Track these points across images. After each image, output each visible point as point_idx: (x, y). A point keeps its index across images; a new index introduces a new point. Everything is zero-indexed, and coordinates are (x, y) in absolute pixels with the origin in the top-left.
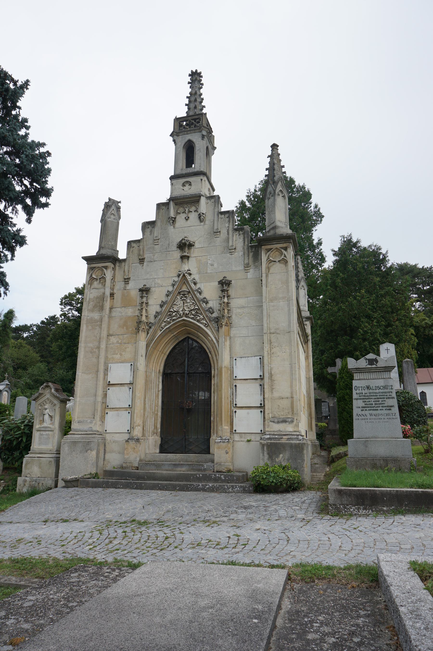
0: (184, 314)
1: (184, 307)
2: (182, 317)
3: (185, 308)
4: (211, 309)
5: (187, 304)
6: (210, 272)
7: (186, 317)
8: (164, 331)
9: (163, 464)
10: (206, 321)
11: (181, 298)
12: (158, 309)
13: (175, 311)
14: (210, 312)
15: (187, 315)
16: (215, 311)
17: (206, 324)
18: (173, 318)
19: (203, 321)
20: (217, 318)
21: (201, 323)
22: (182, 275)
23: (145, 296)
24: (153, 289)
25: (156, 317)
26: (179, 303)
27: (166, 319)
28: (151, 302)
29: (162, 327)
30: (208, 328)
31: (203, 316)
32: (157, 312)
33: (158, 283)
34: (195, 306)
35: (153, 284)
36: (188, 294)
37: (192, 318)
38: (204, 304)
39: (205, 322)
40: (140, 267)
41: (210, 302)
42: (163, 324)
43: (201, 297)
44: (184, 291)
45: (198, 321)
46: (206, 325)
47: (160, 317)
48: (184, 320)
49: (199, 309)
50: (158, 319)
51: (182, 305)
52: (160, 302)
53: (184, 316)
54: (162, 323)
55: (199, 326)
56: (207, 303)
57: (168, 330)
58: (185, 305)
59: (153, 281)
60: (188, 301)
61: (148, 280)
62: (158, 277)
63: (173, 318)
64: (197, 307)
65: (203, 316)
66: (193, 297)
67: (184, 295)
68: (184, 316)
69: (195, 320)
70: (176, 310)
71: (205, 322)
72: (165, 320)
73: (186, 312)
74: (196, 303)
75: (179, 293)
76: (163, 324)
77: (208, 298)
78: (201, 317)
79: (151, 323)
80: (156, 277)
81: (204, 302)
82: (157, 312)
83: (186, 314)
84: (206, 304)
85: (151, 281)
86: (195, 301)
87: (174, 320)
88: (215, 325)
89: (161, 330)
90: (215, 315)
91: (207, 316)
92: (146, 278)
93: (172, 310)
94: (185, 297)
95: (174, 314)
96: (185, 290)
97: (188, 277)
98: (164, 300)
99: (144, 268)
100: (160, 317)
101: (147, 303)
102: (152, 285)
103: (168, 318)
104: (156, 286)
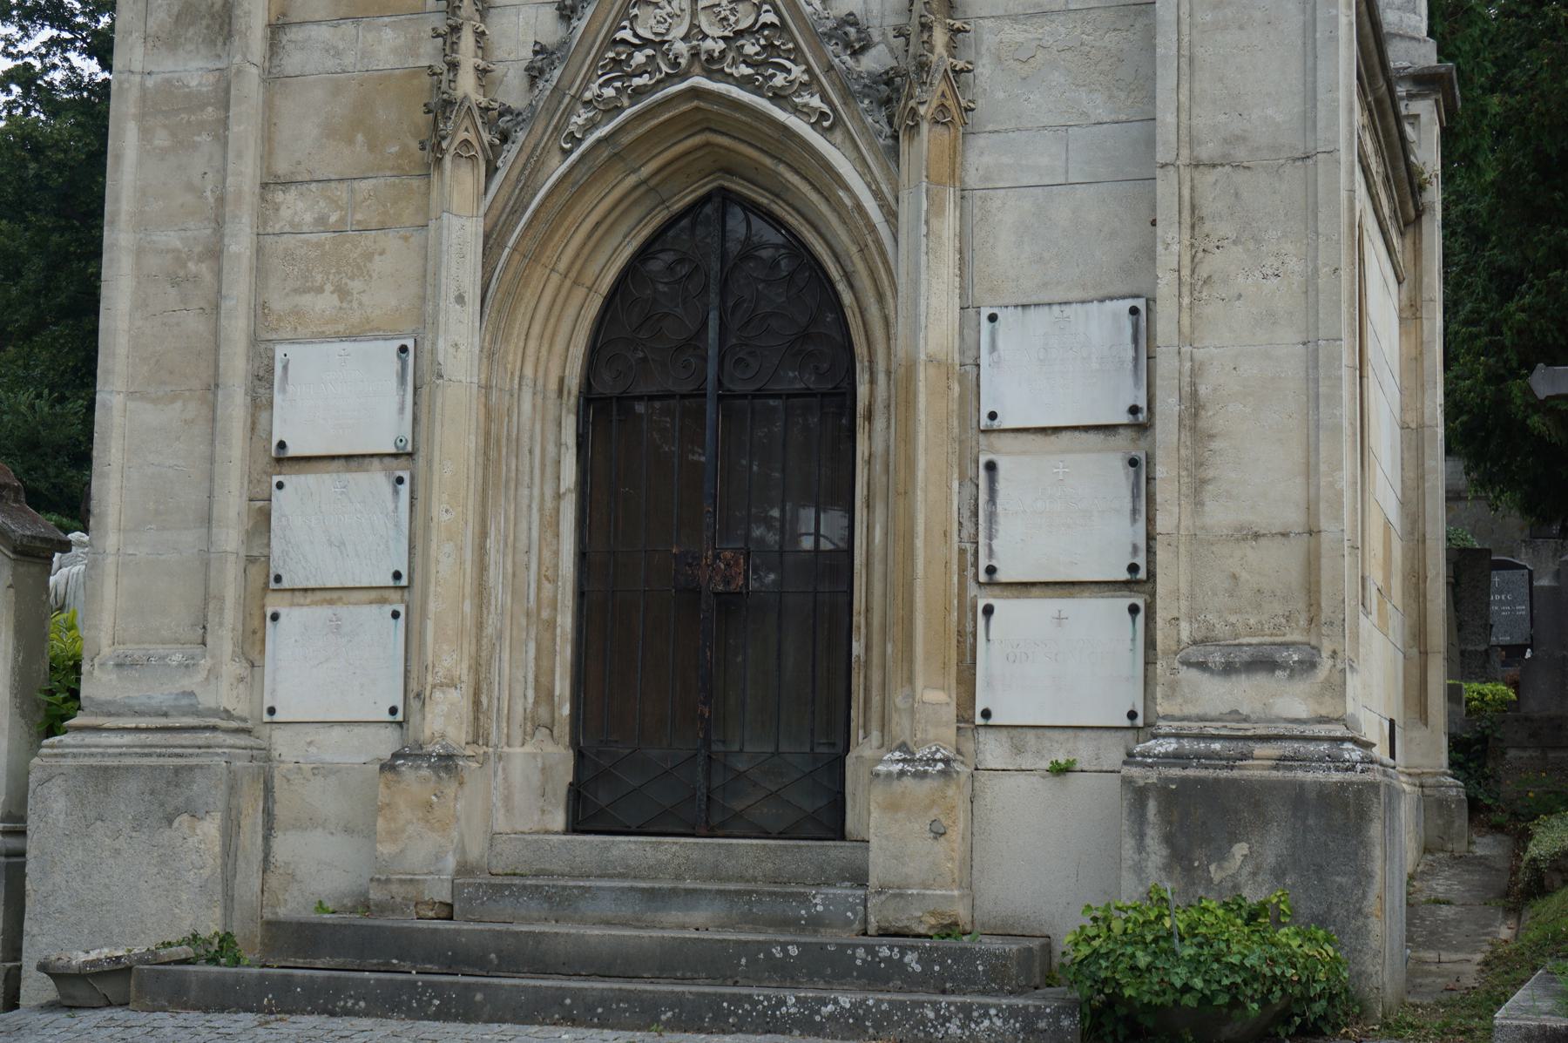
0: (695, 55)
1: (694, 14)
2: (685, 76)
4: (855, 24)
7: (709, 74)
8: (583, 157)
10: (825, 98)
13: (646, 43)
15: (711, 65)
17: (823, 115)
18: (637, 81)
21: (797, 110)
25: (534, 75)
27: (595, 87)
30: (838, 136)
31: (809, 71)
32: (540, 50)
37: (744, 82)
39: (816, 102)
42: (580, 118)
45: (778, 97)
46: (819, 120)
47: (557, 73)
48: (695, 92)
49: (782, 28)
50: (545, 87)
53: (697, 69)
54: (569, 112)
55: (785, 128)
63: (637, 81)
64: (770, 18)
65: (809, 71)
68: (697, 69)
69: (758, 91)
70: (648, 35)
71: (816, 102)
72: (588, 95)
76: (580, 118)
78: (797, 72)
82: (540, 50)
83: (711, 59)
87: (639, 93)
88: (876, 120)
90: (875, 61)
91: (830, 68)
93: (626, 34)
95: (639, 58)
100: (557, 73)
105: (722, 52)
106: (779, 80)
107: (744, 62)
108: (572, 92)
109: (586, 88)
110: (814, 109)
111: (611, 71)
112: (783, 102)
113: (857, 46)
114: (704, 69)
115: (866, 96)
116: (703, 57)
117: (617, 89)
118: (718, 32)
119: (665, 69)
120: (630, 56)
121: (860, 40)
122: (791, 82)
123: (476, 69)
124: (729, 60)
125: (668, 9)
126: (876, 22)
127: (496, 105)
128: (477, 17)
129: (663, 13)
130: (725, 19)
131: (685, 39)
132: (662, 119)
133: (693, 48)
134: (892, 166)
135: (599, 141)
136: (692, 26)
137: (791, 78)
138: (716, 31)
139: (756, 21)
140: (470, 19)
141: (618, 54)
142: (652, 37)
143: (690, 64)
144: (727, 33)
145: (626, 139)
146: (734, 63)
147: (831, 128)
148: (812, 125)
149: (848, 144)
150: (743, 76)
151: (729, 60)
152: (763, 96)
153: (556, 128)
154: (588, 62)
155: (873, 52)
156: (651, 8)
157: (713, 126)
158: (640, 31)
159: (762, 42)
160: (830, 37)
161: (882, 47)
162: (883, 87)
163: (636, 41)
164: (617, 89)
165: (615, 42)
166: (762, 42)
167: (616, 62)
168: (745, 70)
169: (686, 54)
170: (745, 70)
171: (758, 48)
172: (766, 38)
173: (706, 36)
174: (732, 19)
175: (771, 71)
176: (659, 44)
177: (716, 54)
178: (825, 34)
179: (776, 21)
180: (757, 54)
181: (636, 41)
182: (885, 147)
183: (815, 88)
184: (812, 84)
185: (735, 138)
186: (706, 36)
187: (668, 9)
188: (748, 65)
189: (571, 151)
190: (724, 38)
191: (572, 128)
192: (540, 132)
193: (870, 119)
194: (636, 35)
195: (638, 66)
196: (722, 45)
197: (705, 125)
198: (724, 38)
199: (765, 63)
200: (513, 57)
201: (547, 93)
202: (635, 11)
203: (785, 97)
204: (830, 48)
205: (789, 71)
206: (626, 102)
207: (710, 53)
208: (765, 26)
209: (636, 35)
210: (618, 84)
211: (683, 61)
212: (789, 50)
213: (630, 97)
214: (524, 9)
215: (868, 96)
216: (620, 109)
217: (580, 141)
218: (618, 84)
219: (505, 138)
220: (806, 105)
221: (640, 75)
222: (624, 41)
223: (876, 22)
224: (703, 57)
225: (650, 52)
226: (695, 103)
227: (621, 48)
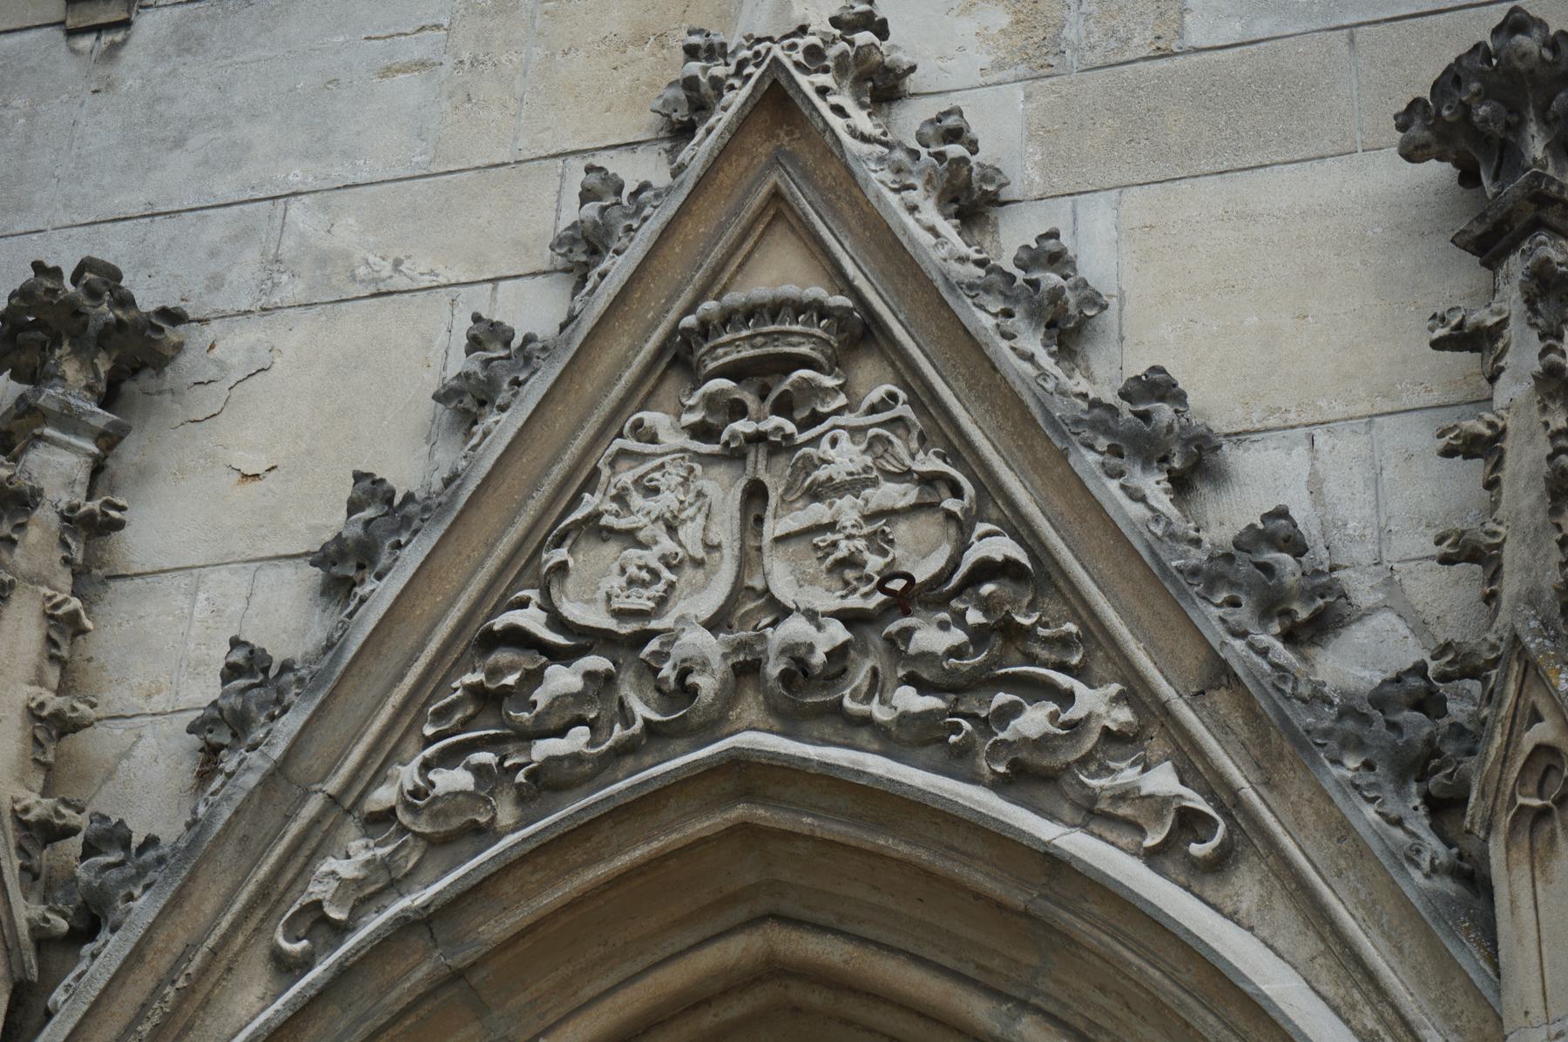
0: (746, 670)
1: (748, 559)
2: (711, 728)
3: (781, 578)
4: (1296, 546)
5: (818, 512)
6: (1233, 31)
7: (790, 720)
8: (343, 973)
9: (276, 997)
10: (1192, 764)
11: (702, 432)
12: (286, 618)
13: (588, 639)
14: (1272, 605)
15: (804, 692)
16: (1362, 588)
17: (1189, 823)
18: (544, 748)
19: (1128, 774)
20: (1417, 692)
21: (1091, 814)
22: (737, 98)
23: (69, 420)
24: (229, 346)
25: (220, 733)
26: (666, 501)
27: (407, 774)
28: (154, 530)
29: (315, 921)
30: (1246, 886)
31: (1135, 692)
32: (247, 664)
33: (323, 260)
34: (962, 527)
35: (245, 270)
36: (836, 362)
37: (908, 738)
38: (1154, 485)
39: (1163, 780)
40: (69, 68)
41: (1236, 458)
42: (352, 857)
43: (1104, 375)
44: (776, 309)
45: (1027, 775)
46: (1178, 842)
47: (290, 724)
48: (745, 774)
49: (1036, 574)
50: (247, 769)
51: (726, 530)
52: (330, 519)
53: (750, 707)
54: (314, 845)
55: (1054, 863)
56: (1195, 466)
57: (419, 970)
58: (774, 527)
59: (244, 235)
60: (845, 458)
61: (162, 227)
62: (341, 172)
63: (544, 748)
64: (1003, 548)
65: (1135, 692)
66: (924, 399)
67: (749, 379)
68: (750, 707)
69: (958, 762)
70: (598, 618)
71: (1163, 780)
72: (384, 796)
73: (796, 628)
74: (989, 488)
75: (680, 357)
76: (352, 857)
77: (1211, 399)
78: (1095, 702)
79: (110, 836)
80: (297, 177)
81: (1141, 445)
82: (247, 664)
83: (798, 670)
84: (1181, 485)
85: (217, 227)
86: (958, 449)
87: (548, 783)
88: (1385, 817)
89: (287, 967)
90: (1353, 663)
91: (1219, 674)
92: (133, 201)
93: (532, 620)
94: (784, 407)
95: (563, 679)
96: (790, 290)
97: (848, 118)
98: (407, 472)
99: (131, 83)
100: (290, 724)
101: (93, 527)
102: (216, 282)
103: (448, 758)
104: (292, 289)
105: (838, 654)
106: (1034, 720)
107: (912, 680)
108: (333, 786)
109: (379, 778)
110: (1158, 804)
111: (465, 725)
112: (1043, 795)
113: (1303, 614)
114: (773, 709)
115: (1355, 744)
116: (774, 669)
117: (479, 771)
118: (827, 599)
119: (642, 711)
120: (534, 678)
121: (1309, 595)
122: (1076, 728)
123: (34, 714)
124: (861, 678)
125: (667, 545)
126: (1362, 553)
127: (82, 820)
128: (64, 580)
129: (651, 557)
130: (851, 562)
131: (715, 624)
132: (623, 861)
133: (741, 646)
134: (1469, 959)
135: (406, 925)
136: (739, 591)
137: (1075, 713)
138: (827, 599)
139: (954, 563)
140: (35, 580)
141: (494, 673)
142: (609, 623)
143: (729, 697)
144: (854, 602)
145: (494, 928)
146: (876, 685)
147: (1219, 864)
148: (1152, 857)
149: (1283, 912)
150: (905, 718)
151: (861, 678)
152: (974, 779)
153: (263, 892)
154: (396, 698)
155: (1357, 635)
156: (611, 549)
157: (788, 906)
158: (573, 611)
159: (974, 617)
160: (1213, 581)
161: (1385, 621)
162: (1407, 716)
163: (559, 639)
164: (479, 771)
165: (490, 641)
166: (974, 617)
167: (487, 699)
168: (910, 700)
169: (716, 663)
170: (910, 700)
171: (957, 636)
172: (985, 605)
173: (782, 612)
174: (874, 563)
175: (1002, 698)
176: (628, 643)
177: (818, 658)
178: (1195, 572)
179: (1021, 556)
180: (956, 652)
181: (559, 639)
182: (1430, 897)
183: (1157, 746)
184: (1150, 725)
185: (863, 941)
186: (782, 612)
187: (667, 545)
188: (924, 688)
189: (306, 962)
190: (849, 618)
191: (318, 890)
192: (209, 907)
193: (1370, 812)
194: (558, 622)
195: (558, 701)
196: (838, 633)
197: (764, 904)
198: (849, 618)
199: (984, 681)
200: (158, 703)
201: (251, 780)
202: (561, 554)
203: (1049, 778)
204: (1210, 616)
205: (1067, 698)
206: (506, 813)
207: (797, 656)
208: (987, 570)
209: (558, 622)
210: (486, 757)
211: (707, 684)
212: (1065, 642)
213: (523, 798)
214: (214, 576)
215: (1359, 745)
216: (483, 833)
217: (341, 930)
218: (486, 757)
219: (90, 922)
220: (1123, 796)
221: (561, 733)
222: (519, 638)
223: (1362, 553)
224: (774, 669)
225: (597, 662)
226: (739, 812)
227: (503, 656)
